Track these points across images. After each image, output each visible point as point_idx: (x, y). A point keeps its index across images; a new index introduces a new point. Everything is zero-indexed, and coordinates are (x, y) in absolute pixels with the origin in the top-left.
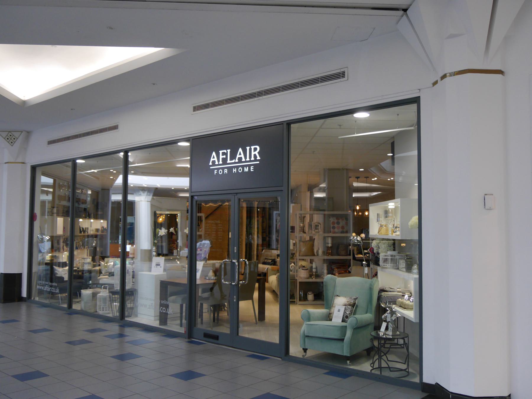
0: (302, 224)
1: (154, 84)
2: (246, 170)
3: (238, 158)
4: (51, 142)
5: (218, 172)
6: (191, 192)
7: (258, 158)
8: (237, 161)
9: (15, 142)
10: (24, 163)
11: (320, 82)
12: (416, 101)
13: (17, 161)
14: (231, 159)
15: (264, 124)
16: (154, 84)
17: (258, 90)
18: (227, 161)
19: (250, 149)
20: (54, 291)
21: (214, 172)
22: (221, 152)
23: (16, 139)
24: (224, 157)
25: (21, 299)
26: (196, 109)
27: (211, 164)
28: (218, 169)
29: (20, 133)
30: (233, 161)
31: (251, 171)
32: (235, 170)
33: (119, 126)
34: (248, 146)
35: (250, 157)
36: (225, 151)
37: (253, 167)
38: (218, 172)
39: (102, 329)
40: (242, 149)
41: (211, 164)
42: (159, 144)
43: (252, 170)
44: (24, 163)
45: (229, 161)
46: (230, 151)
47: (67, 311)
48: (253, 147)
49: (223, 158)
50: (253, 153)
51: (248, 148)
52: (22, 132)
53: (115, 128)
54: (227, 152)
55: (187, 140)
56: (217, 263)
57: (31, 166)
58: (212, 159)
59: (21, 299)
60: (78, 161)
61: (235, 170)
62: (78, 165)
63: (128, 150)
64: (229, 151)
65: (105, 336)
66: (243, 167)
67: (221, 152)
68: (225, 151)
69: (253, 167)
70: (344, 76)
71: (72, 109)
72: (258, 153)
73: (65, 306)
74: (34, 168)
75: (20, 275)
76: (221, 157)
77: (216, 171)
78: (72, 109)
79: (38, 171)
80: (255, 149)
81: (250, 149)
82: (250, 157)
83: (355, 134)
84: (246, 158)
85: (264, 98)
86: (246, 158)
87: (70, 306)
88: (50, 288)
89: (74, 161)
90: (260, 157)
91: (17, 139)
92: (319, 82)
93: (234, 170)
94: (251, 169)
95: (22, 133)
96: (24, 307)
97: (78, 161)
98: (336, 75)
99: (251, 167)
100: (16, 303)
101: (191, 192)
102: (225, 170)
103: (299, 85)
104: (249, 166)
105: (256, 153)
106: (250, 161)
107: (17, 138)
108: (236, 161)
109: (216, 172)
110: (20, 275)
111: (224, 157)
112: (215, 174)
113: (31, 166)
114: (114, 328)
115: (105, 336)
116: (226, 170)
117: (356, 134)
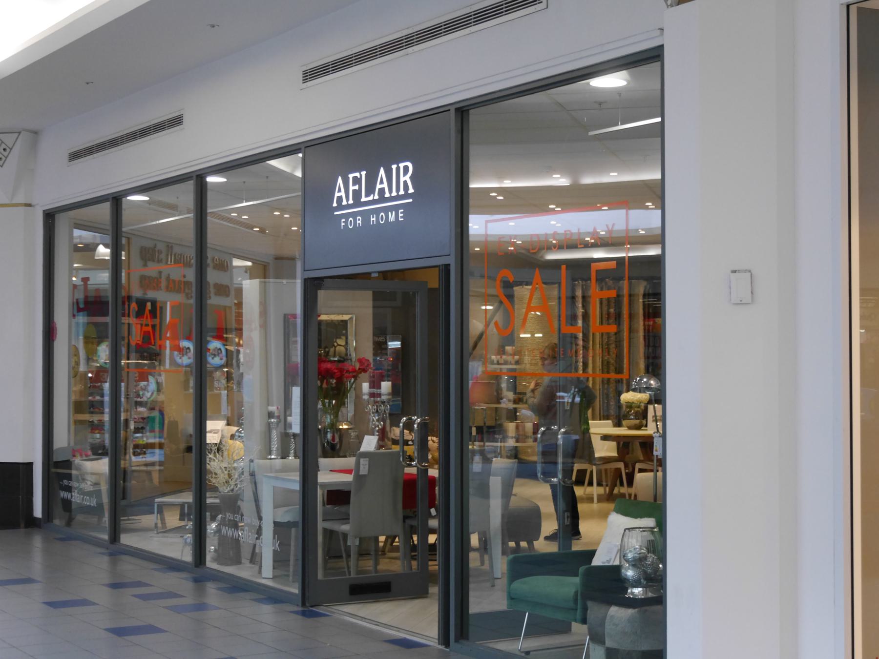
0: (321, 351)
1: (213, 26)
2: (392, 217)
3: (379, 189)
4: (75, 156)
5: (346, 222)
6: (304, 271)
7: (411, 190)
8: (376, 197)
9: (6, 158)
10: (30, 205)
11: (473, 24)
12: (300, 149)
13: (14, 202)
14: (367, 195)
15: (342, 131)
16: (213, 26)
17: (405, 33)
18: (361, 197)
19: (398, 169)
20: (88, 504)
21: (341, 223)
22: (351, 176)
23: (8, 150)
24: (357, 187)
25: (32, 523)
26: (311, 75)
27: (335, 205)
28: (346, 216)
29: (17, 135)
30: (371, 198)
31: (400, 219)
32: (374, 219)
33: (184, 116)
34: (394, 164)
35: (398, 190)
36: (357, 174)
37: (402, 211)
38: (346, 222)
39: (145, 583)
40: (342, 179)
41: (335, 205)
42: (169, 181)
43: (401, 217)
44: (30, 205)
45: (364, 199)
46: (365, 174)
47: (107, 549)
48: (402, 165)
49: (354, 191)
50: (402, 179)
51: (394, 167)
52: (19, 133)
53: (176, 121)
54: (361, 175)
55: (141, 190)
56: (565, 436)
57: (44, 211)
58: (337, 194)
59: (32, 523)
60: (210, 179)
61: (373, 219)
62: (209, 187)
63: (120, 196)
64: (364, 173)
65: (135, 596)
66: (386, 210)
67: (351, 176)
68: (357, 174)
69: (402, 211)
70: (305, 73)
71: (88, 83)
72: (411, 178)
73: (106, 537)
74: (50, 217)
75: (29, 466)
76: (352, 188)
77: (401, 213)
78: (88, 83)
79: (62, 223)
80: (406, 169)
81: (398, 169)
82: (398, 190)
83: (617, 125)
84: (391, 191)
85: (415, 50)
86: (391, 191)
87: (114, 538)
88: (82, 496)
89: (199, 178)
90: (414, 188)
91: (11, 149)
92: (471, 23)
93: (372, 219)
94: (400, 215)
95: (21, 135)
96: (37, 541)
97: (210, 179)
98: (465, 18)
99: (400, 211)
100: (22, 531)
101: (304, 271)
102: (358, 218)
103: (502, 9)
104: (396, 208)
105: (407, 178)
106: (398, 197)
107: (11, 147)
108: (375, 198)
109: (344, 224)
110: (29, 466)
111: (357, 187)
112: (342, 228)
113: (44, 211)
114: (179, 583)
115: (135, 596)
116: (359, 219)
117: (622, 124)
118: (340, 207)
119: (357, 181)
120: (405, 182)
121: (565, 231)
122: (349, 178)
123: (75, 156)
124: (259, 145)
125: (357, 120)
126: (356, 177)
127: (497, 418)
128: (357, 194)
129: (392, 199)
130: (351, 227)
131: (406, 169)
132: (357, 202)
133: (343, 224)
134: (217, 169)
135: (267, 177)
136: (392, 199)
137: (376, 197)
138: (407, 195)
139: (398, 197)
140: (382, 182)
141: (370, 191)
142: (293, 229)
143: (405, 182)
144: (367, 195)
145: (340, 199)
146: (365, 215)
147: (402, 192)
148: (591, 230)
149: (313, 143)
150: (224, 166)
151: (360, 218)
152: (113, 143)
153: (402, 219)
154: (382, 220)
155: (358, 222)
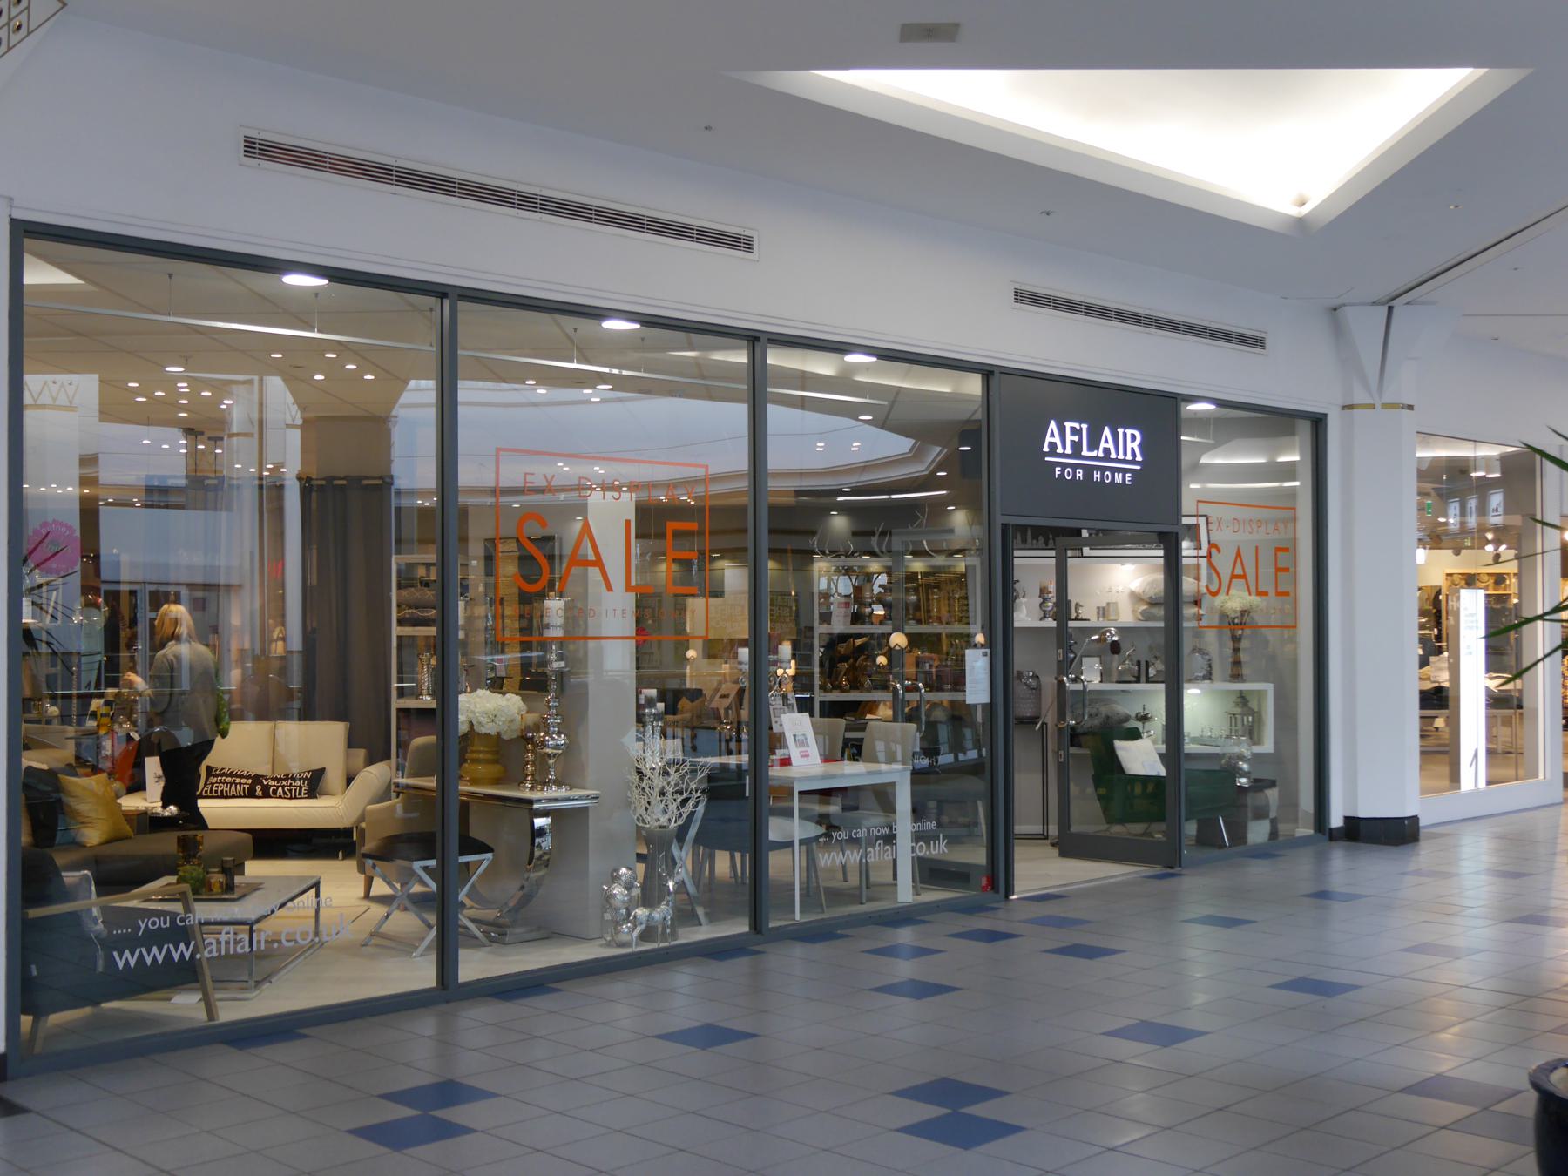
2: (1118, 479)
4: (256, 148)
5: (1063, 471)
7: (1139, 458)
8: (1101, 454)
17: (1147, 312)
23: (23, 31)
27: (1046, 449)
30: (1094, 454)
31: (1127, 483)
34: (1122, 427)
38: (1063, 471)
44: (1351, 407)
48: (1129, 432)
49: (1073, 442)
50: (1130, 445)
58: (1048, 439)
64: (1085, 427)
66: (1113, 470)
67: (1068, 425)
68: (1077, 426)
72: (1140, 446)
84: (1117, 453)
93: (1095, 476)
94: (1127, 479)
99: (1127, 475)
102: (1078, 470)
104: (1125, 471)
105: (1135, 445)
106: (1124, 461)
111: (1076, 438)
118: (1053, 452)
119: (1074, 431)
120: (1133, 449)
121: (580, 478)
122: (1065, 427)
123: (256, 148)
124: (907, 341)
125: (954, 351)
126: (1075, 428)
127: (1031, 674)
128: (1077, 446)
129: (1117, 460)
130: (1107, 481)
131: (1134, 438)
132: (1076, 451)
133: (1057, 473)
134: (645, 320)
135: (170, 275)
136: (1117, 460)
137: (1101, 454)
138: (1133, 462)
139: (1124, 461)
140: (1052, 435)
141: (1094, 445)
142: (203, 394)
143: (1133, 449)
144: (1090, 449)
145: (1053, 446)
146: (1089, 470)
147: (1129, 457)
148: (601, 482)
149: (1036, 375)
150: (654, 320)
151: (1080, 471)
152: (529, 202)
153: (1130, 483)
154: (1069, 472)
155: (1078, 475)
